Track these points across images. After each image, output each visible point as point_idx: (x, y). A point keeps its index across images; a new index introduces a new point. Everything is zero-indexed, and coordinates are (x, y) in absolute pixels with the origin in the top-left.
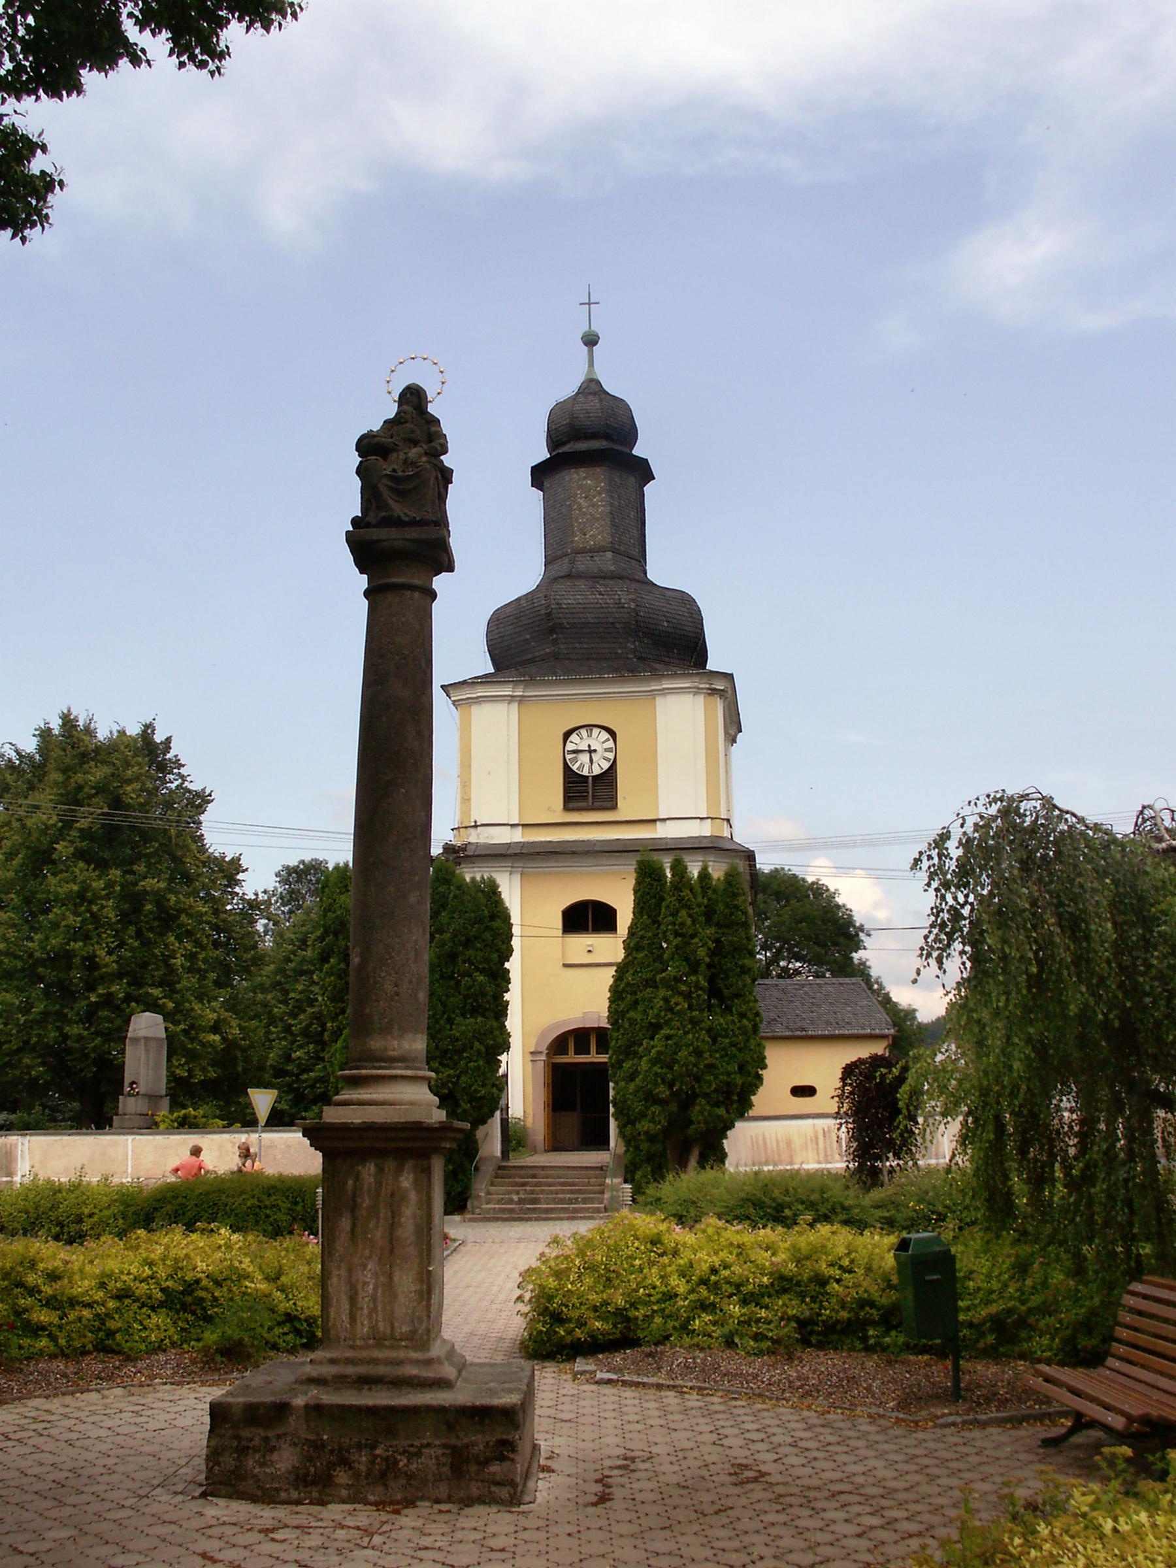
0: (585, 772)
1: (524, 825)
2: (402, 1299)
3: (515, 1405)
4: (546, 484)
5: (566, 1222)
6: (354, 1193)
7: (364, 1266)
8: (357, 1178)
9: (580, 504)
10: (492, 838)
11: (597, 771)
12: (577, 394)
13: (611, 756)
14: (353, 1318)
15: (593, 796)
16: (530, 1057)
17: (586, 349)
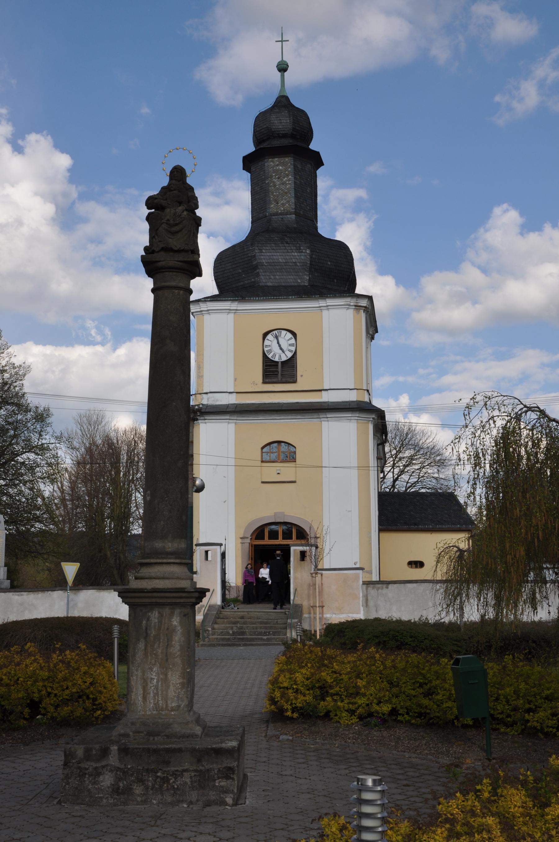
0: (277, 359)
1: (237, 393)
2: (172, 688)
3: (235, 747)
4: (253, 169)
5: (262, 647)
6: (146, 629)
7: (151, 669)
8: (148, 620)
9: (274, 182)
10: (217, 400)
11: (284, 358)
12: (273, 107)
13: (293, 349)
14: (145, 698)
15: (282, 375)
16: (240, 541)
17: (279, 74)
